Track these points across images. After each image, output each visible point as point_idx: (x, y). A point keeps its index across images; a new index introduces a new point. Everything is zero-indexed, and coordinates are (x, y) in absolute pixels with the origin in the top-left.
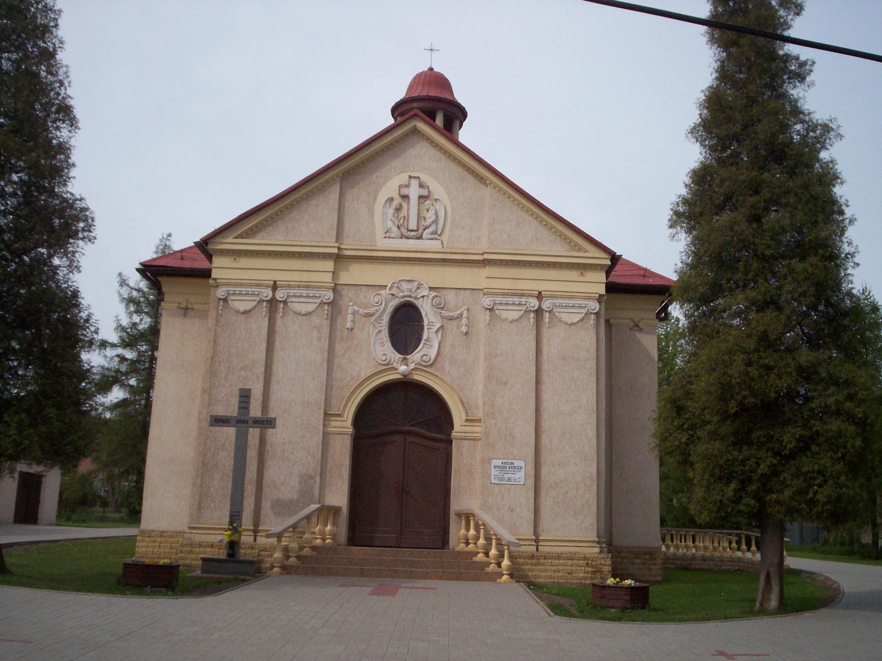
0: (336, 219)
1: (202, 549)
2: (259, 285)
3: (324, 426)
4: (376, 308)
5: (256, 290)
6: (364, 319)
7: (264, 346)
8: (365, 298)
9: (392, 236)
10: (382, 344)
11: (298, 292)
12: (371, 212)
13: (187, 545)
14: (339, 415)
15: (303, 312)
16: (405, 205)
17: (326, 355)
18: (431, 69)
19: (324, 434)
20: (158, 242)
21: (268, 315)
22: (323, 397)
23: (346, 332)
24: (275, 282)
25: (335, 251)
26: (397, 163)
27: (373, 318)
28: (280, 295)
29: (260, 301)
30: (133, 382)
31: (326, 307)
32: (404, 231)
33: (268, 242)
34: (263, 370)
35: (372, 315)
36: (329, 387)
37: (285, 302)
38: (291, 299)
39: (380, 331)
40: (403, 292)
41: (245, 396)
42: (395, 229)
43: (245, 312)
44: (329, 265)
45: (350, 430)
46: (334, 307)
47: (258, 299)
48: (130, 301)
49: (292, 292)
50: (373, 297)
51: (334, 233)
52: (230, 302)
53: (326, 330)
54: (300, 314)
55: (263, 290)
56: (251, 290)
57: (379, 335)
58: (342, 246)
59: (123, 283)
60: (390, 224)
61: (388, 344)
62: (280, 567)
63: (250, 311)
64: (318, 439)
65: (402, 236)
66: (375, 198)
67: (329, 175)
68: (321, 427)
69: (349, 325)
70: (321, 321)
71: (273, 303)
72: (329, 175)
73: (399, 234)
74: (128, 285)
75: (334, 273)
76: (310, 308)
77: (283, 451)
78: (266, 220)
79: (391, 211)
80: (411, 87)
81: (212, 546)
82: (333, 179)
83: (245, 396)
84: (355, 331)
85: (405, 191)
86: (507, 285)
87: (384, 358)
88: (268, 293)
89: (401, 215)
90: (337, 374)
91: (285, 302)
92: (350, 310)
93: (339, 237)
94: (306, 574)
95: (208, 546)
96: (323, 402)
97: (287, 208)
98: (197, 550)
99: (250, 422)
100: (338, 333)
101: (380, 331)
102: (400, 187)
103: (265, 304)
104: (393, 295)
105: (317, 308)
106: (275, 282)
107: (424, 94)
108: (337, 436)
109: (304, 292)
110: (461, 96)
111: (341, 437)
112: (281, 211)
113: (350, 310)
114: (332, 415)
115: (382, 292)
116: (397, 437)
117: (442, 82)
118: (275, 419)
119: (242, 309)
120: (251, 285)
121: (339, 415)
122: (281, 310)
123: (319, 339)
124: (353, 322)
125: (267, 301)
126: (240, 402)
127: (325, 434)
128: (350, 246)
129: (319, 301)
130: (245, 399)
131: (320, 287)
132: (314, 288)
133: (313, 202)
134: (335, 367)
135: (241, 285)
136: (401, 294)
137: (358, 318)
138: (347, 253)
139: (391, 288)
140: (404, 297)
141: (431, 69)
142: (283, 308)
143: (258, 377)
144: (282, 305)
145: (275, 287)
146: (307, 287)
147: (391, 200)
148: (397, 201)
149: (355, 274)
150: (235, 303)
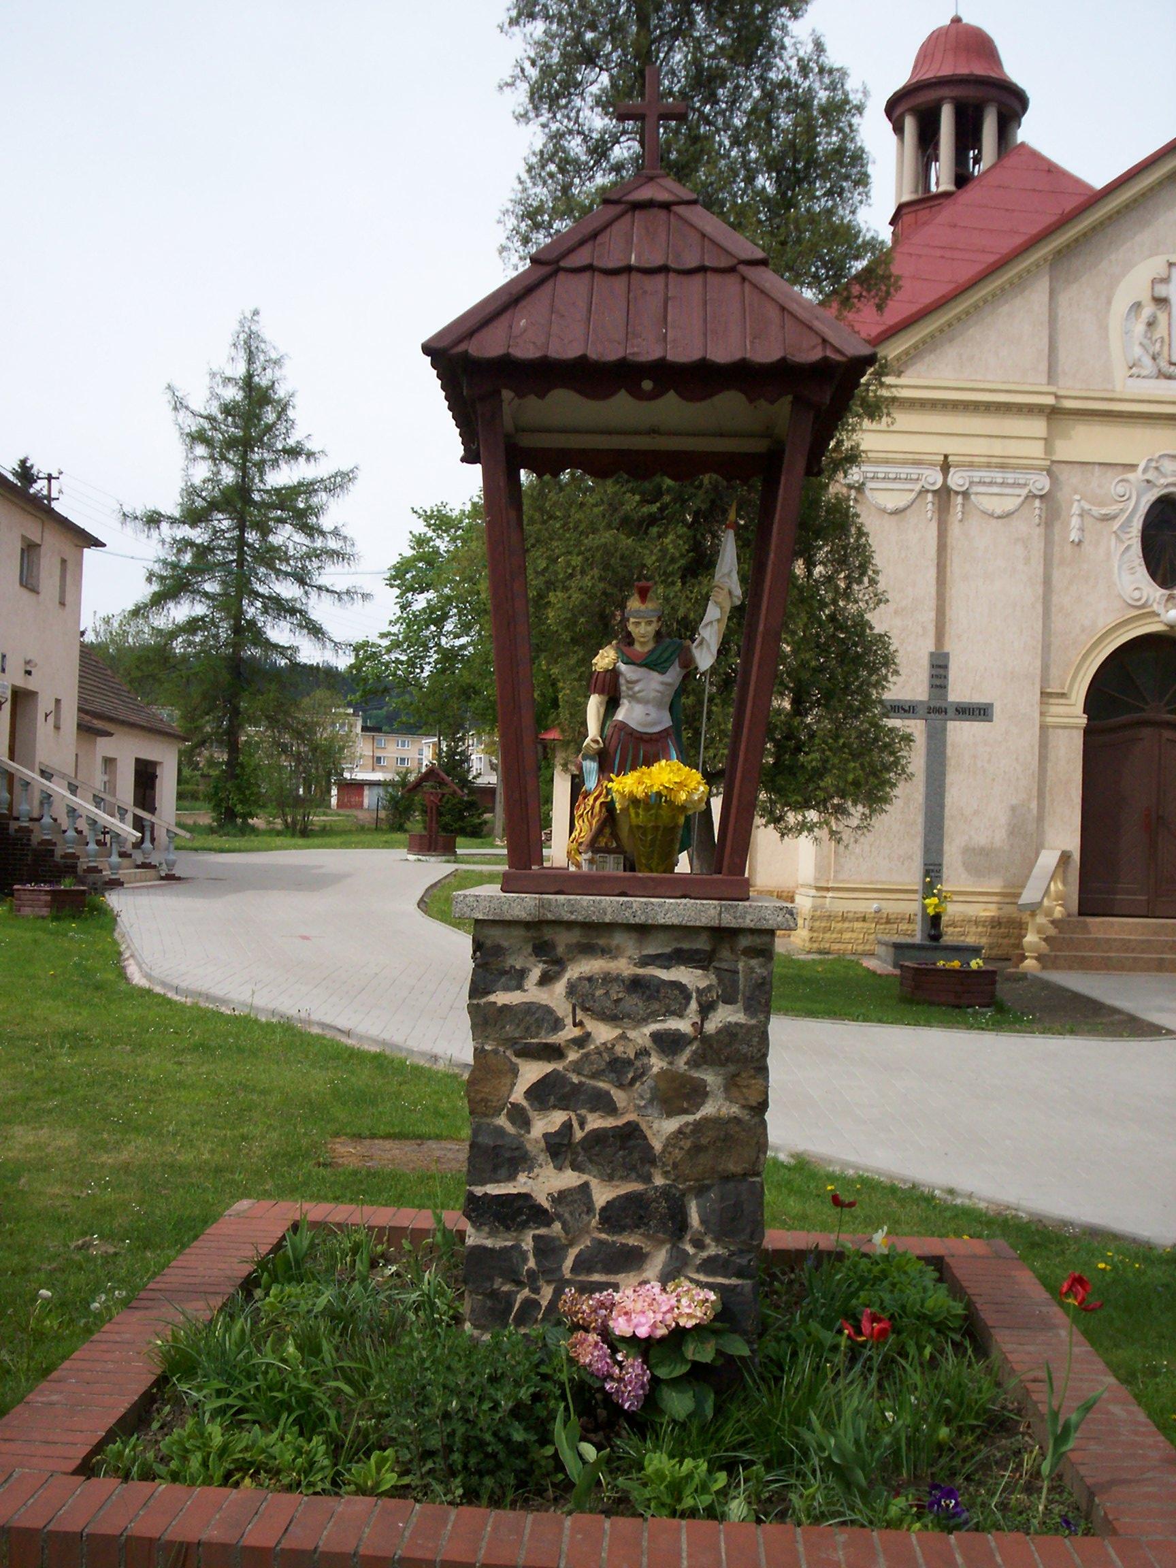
0: (1046, 340)
1: (846, 925)
2: (917, 463)
3: (1042, 714)
4: (1121, 506)
5: (913, 471)
6: (1099, 525)
7: (932, 573)
8: (1100, 486)
9: (1144, 373)
10: (1132, 570)
11: (986, 475)
12: (1103, 328)
13: (821, 918)
14: (1063, 695)
15: (998, 512)
16: (1162, 317)
17: (1040, 591)
18: (957, 20)
19: (1041, 727)
20: (237, 327)
21: (936, 516)
22: (1038, 663)
23: (1068, 549)
24: (946, 456)
25: (1050, 400)
26: (1145, 237)
27: (1116, 525)
28: (956, 480)
29: (920, 492)
30: (211, 587)
31: (1037, 503)
32: (1163, 364)
33: (932, 383)
34: (933, 615)
35: (1114, 517)
36: (1046, 647)
37: (966, 494)
38: (975, 489)
39: (1128, 547)
40: (1165, 476)
41: (940, 667)
42: (1147, 360)
43: (896, 512)
44: (1038, 427)
45: (1083, 720)
46: (1049, 505)
47: (918, 487)
48: (199, 437)
49: (977, 475)
50: (1113, 485)
51: (1044, 366)
52: (867, 492)
53: (1038, 546)
54: (991, 515)
55: (927, 472)
56: (904, 471)
57: (1126, 557)
58: (1061, 393)
59: (179, 405)
60: (1137, 351)
61: (1142, 571)
62: (1037, 959)
63: (904, 510)
64: (1032, 736)
65: (1162, 375)
66: (1109, 302)
67: (1032, 259)
68: (1037, 715)
69: (1074, 536)
70: (1028, 526)
71: (944, 494)
72: (1032, 259)
73: (1155, 371)
74: (187, 408)
75: (1048, 441)
76: (1010, 504)
77: (975, 757)
78: (924, 342)
79: (1140, 328)
80: (927, 53)
81: (864, 919)
82: (1038, 266)
83: (940, 667)
84: (1085, 544)
85: (1162, 291)
86: (998, 448)
87: (1137, 594)
88: (934, 478)
89: (1157, 335)
90: (1058, 623)
91: (966, 494)
92: (1075, 509)
93: (1052, 375)
94: (1070, 968)
95: (857, 920)
96: (1038, 672)
97: (959, 319)
98: (840, 925)
99: (922, 711)
100: (1056, 549)
101: (1128, 547)
102: (1153, 281)
103: (930, 497)
104: (1148, 481)
105: (1023, 502)
106: (946, 456)
107: (963, 70)
108: (1060, 731)
109: (998, 476)
110: (1015, 70)
111: (1067, 732)
112: (950, 325)
113: (1075, 509)
114: (1050, 695)
115: (1131, 476)
116: (1146, 732)
117: (978, 44)
118: (991, 705)
119: (891, 506)
120: (904, 463)
121: (1063, 695)
122: (959, 508)
123: (1027, 560)
124: (1082, 529)
125: (934, 492)
126: (945, 677)
127: (1044, 728)
128: (1073, 389)
129: (1024, 492)
130: (941, 671)
131: (1027, 467)
132: (1015, 468)
133: (1005, 309)
134: (1053, 609)
135: (886, 462)
136: (1163, 481)
137: (1088, 520)
138: (1069, 404)
139: (1145, 471)
140: (1167, 486)
141: (957, 20)
142: (963, 505)
143: (924, 628)
144: (960, 499)
145: (946, 467)
146: (1003, 467)
147: (1138, 306)
148: (1148, 310)
149: (1085, 443)
150: (876, 493)
